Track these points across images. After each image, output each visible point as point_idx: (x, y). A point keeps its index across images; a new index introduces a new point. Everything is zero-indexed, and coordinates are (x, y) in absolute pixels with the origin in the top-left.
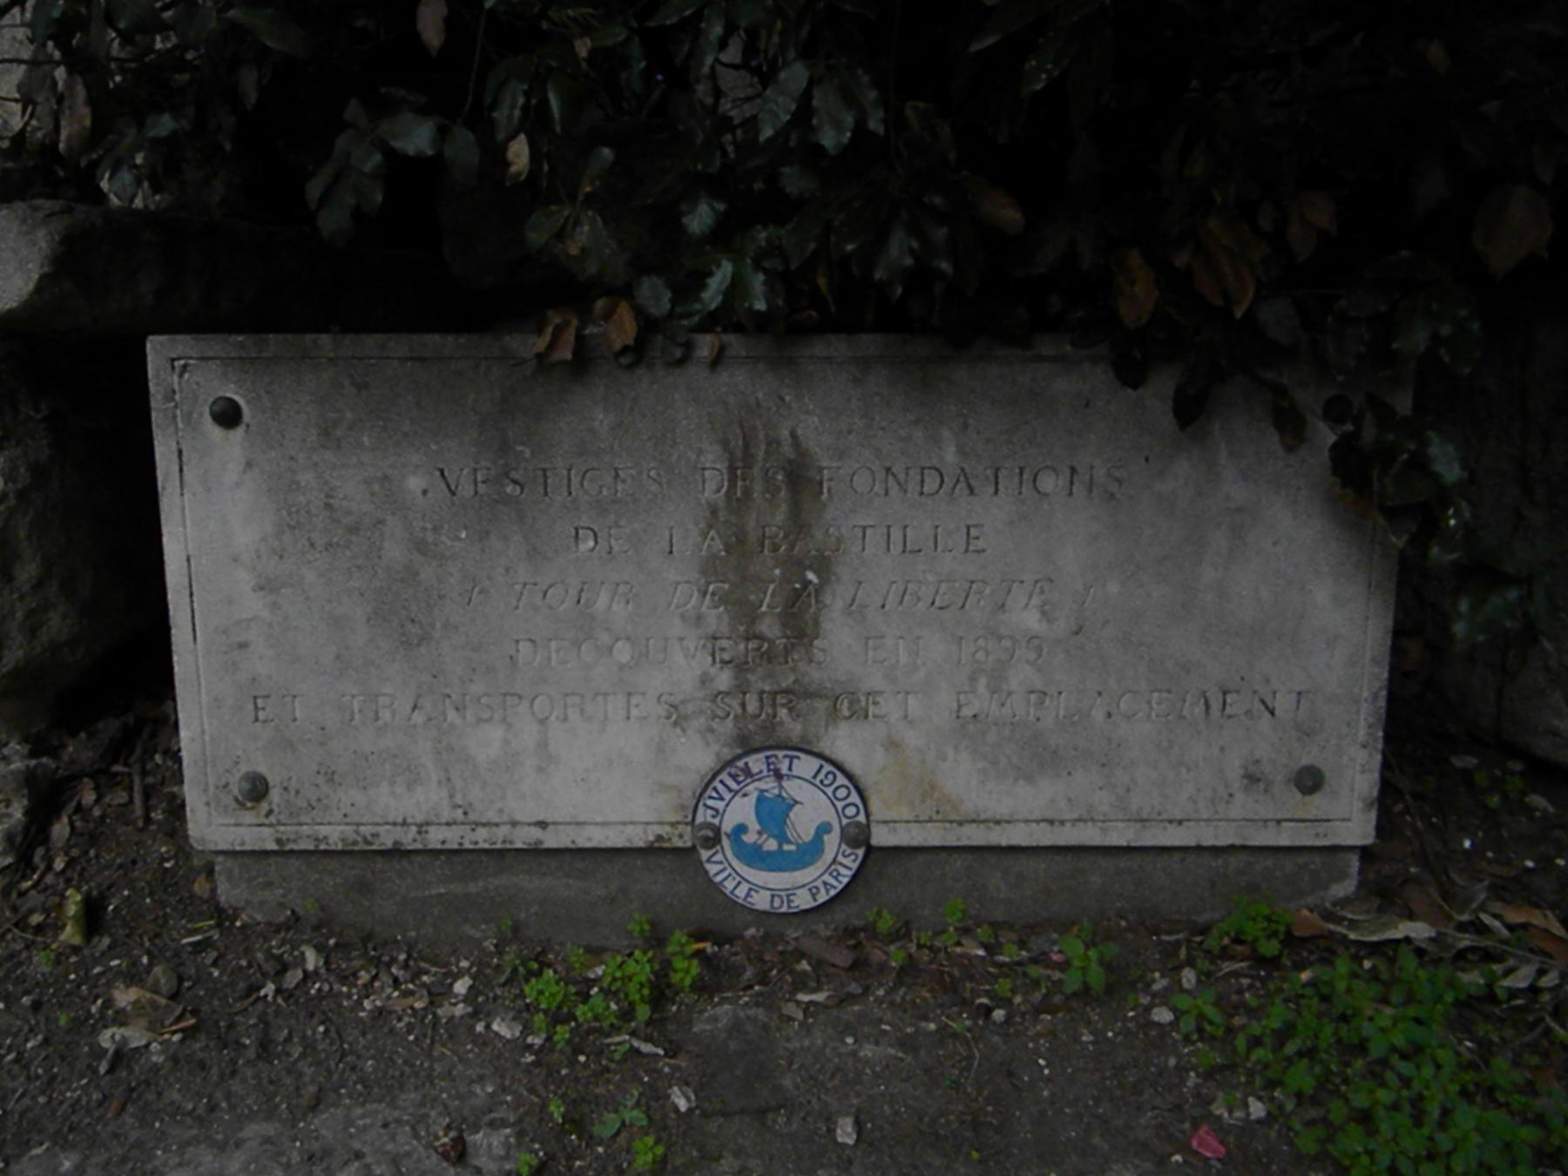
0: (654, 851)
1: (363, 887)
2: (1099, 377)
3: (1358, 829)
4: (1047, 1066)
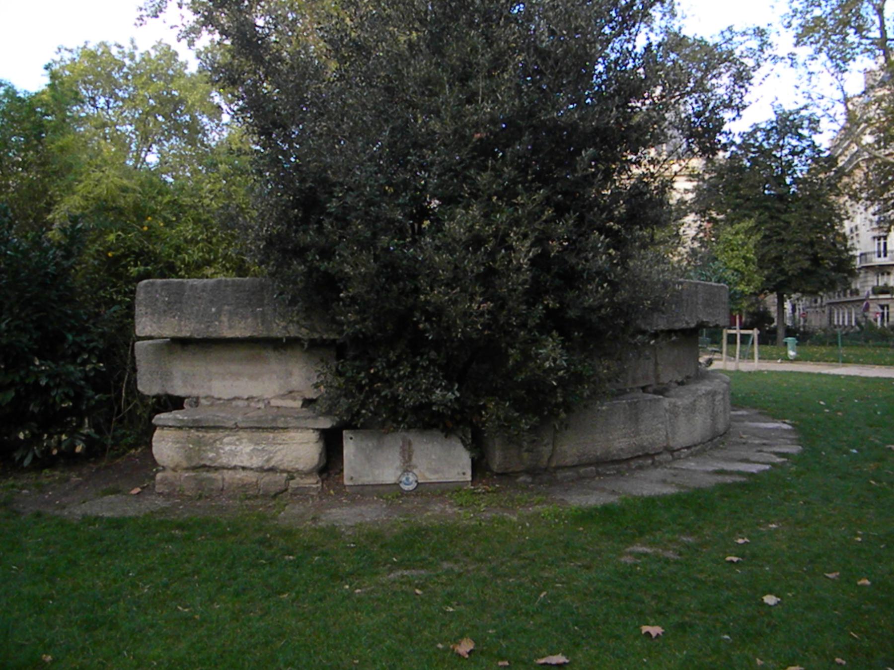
0: (395, 484)
2: (443, 435)
3: (470, 479)
4: (399, 375)
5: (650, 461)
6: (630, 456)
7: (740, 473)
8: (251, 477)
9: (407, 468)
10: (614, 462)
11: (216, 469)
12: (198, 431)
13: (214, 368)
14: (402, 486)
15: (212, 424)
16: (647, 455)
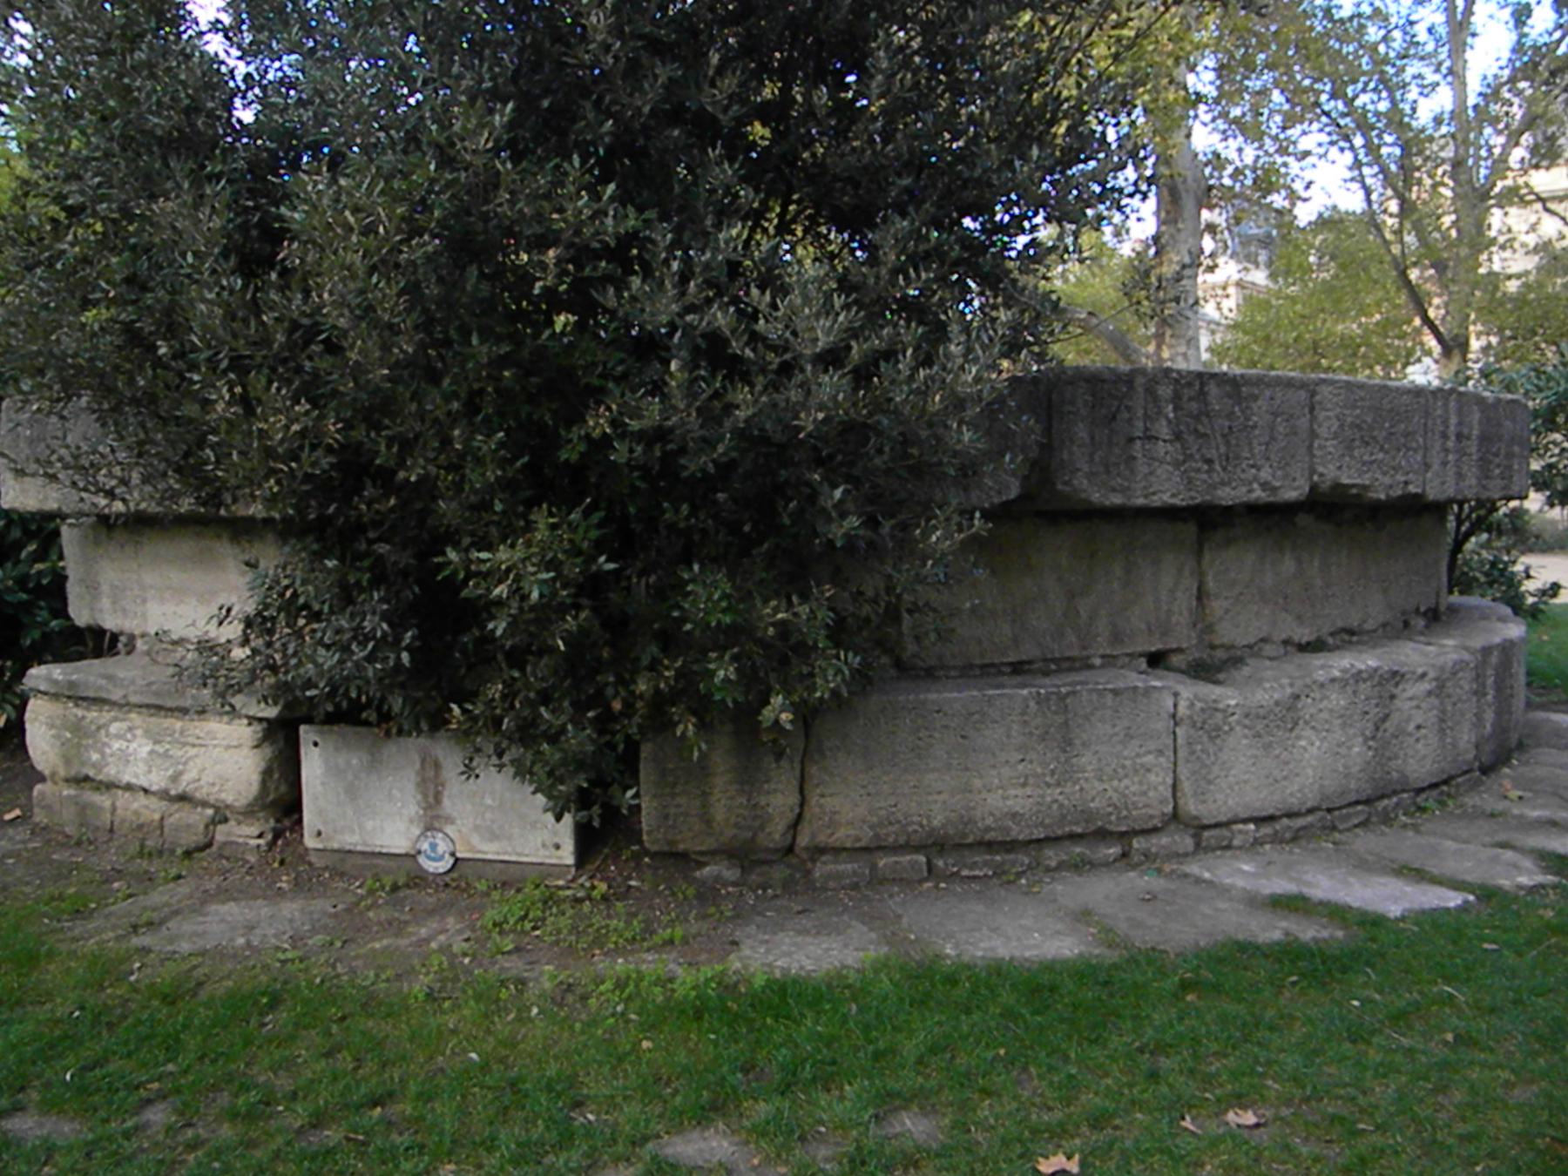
0: (407, 855)
1: (343, 860)
5: (1114, 851)
6: (1039, 833)
7: (1336, 912)
8: (151, 810)
9: (432, 821)
10: (989, 846)
11: (110, 786)
12: (77, 705)
13: (149, 578)
14: (421, 860)
15: (91, 694)
16: (1103, 835)
